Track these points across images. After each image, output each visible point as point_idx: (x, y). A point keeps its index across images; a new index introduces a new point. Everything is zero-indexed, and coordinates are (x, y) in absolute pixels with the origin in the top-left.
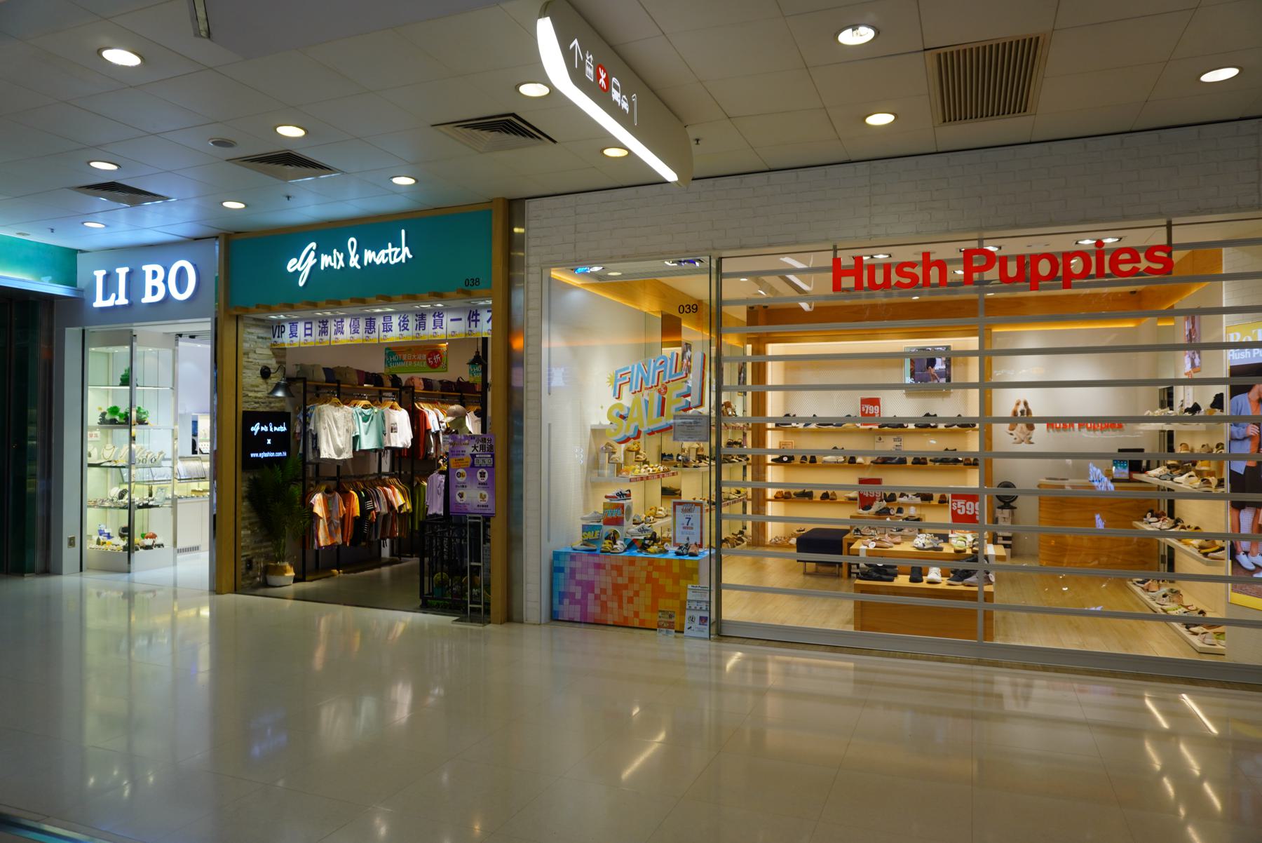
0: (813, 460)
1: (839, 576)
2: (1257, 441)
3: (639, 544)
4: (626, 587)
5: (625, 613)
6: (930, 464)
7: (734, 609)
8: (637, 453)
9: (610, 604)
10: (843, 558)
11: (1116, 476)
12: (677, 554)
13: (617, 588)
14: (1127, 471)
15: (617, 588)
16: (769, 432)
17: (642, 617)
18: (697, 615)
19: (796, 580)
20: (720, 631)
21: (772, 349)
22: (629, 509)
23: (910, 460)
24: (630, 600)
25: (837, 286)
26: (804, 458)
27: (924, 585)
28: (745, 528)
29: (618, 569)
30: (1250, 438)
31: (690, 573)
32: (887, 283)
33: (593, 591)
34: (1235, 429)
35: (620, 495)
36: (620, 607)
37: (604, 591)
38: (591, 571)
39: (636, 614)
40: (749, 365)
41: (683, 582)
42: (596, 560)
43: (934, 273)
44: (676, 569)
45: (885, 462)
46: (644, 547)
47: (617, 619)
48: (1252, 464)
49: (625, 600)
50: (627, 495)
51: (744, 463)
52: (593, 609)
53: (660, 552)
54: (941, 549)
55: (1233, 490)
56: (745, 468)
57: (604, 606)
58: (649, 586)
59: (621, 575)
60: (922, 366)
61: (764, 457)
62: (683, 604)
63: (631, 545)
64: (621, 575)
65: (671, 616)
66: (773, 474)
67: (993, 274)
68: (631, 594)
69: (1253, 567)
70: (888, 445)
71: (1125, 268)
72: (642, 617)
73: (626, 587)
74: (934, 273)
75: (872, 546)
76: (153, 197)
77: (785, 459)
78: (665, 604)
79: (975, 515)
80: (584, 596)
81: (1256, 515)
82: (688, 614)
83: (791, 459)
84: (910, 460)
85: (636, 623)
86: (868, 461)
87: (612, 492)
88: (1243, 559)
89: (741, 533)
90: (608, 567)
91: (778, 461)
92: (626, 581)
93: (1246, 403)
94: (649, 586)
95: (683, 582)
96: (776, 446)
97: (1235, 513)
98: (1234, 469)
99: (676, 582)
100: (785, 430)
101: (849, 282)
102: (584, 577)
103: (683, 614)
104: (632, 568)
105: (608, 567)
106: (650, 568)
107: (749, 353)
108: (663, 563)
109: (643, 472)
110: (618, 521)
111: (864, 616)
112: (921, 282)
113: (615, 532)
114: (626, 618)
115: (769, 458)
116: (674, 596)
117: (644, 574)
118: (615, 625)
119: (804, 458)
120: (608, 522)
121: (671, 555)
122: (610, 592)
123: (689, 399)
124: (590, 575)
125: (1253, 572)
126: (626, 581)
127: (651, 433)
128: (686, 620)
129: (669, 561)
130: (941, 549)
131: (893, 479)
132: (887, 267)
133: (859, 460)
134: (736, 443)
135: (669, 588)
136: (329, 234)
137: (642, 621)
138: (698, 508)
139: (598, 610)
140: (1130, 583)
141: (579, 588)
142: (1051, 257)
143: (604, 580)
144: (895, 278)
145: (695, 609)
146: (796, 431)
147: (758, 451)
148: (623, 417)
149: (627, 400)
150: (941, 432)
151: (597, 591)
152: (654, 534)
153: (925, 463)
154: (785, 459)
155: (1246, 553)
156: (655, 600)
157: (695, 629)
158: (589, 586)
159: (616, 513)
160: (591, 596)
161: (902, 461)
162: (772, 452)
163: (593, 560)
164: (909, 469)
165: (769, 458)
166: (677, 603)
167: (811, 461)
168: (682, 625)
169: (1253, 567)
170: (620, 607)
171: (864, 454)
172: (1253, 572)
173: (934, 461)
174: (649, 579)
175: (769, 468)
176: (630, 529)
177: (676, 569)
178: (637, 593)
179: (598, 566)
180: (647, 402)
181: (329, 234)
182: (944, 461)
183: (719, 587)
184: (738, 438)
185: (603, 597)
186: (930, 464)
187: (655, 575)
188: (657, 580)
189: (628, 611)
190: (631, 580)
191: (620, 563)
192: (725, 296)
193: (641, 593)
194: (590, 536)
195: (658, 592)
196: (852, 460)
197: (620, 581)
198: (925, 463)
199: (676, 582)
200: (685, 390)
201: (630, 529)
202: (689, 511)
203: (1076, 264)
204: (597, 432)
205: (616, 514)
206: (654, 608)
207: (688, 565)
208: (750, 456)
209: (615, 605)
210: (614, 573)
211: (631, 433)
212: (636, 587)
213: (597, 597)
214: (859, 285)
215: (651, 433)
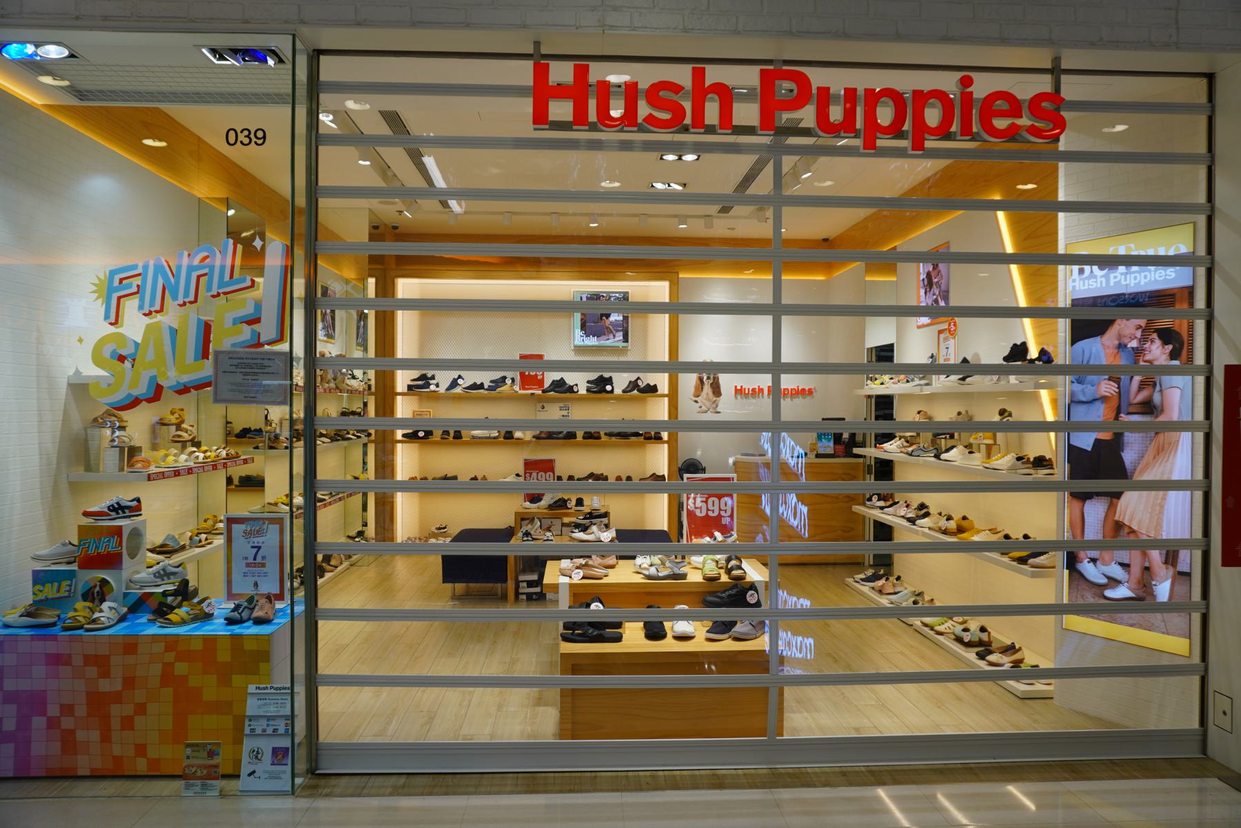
0: (458, 435)
1: (504, 598)
2: (1115, 403)
3: (153, 603)
4: (117, 698)
5: (117, 750)
6: (604, 438)
7: (345, 714)
8: (178, 427)
9: (80, 735)
11: (821, 451)
12: (230, 621)
13: (98, 703)
14: (832, 444)
15: (98, 703)
16: (399, 398)
17: (152, 753)
18: (266, 746)
19: (443, 604)
20: (315, 766)
21: (406, 287)
22: (137, 534)
23: (580, 435)
24: (128, 723)
25: (540, 117)
26: (446, 433)
27: (668, 645)
28: (365, 525)
29: (101, 663)
30: (1104, 399)
31: (252, 659)
32: (630, 118)
33: (43, 713)
34: (1077, 387)
35: (118, 509)
36: (106, 738)
37: (68, 709)
38: (40, 670)
39: (141, 750)
40: (371, 315)
41: (237, 680)
42: (51, 647)
43: (712, 112)
44: (224, 656)
45: (549, 436)
46: (162, 611)
47: (98, 764)
48: (1105, 436)
49: (115, 723)
50: (135, 508)
51: (364, 439)
52: (43, 747)
53: (195, 619)
54: (684, 576)
55: (1073, 475)
56: (365, 445)
57: (69, 743)
58: (168, 693)
59: (105, 674)
60: (595, 317)
61: (393, 433)
62: (240, 720)
63: (138, 605)
64: (105, 674)
65: (211, 754)
66: (406, 461)
67: (807, 116)
68: (128, 710)
69: (1104, 581)
70: (553, 414)
71: (1001, 123)
72: (152, 753)
73: (117, 698)
74: (712, 112)
75: (577, 577)
76: (1080, 713)
77: (421, 434)
78: (203, 727)
79: (720, 517)
80: (24, 723)
81: (1112, 508)
82: (248, 745)
83: (429, 433)
84: (580, 435)
85: (142, 766)
86: (528, 436)
87: (100, 505)
88: (1088, 569)
89: (361, 534)
90: (78, 661)
91: (412, 437)
92: (118, 686)
93: (1099, 349)
94: (168, 693)
95: (237, 680)
96: (408, 415)
97: (1077, 504)
98: (1074, 442)
99: (224, 680)
100: (419, 394)
101: (561, 110)
102: (24, 685)
103: (238, 741)
104: (130, 659)
105: (78, 661)
106: (170, 657)
107: (371, 293)
108: (198, 646)
109: (183, 460)
110: (112, 561)
111: (580, 714)
112: (688, 120)
113: (104, 582)
114: (118, 760)
115: (399, 434)
116: (221, 707)
117: (157, 669)
118: (96, 776)
119: (446, 433)
120: (90, 562)
121: (218, 627)
122: (81, 711)
123: (256, 327)
124: (38, 678)
125: (1104, 587)
126: (118, 686)
127: (183, 390)
128: (245, 758)
129: (210, 641)
130: (684, 576)
131: (574, 461)
132: (631, 91)
133: (518, 434)
134: (353, 413)
135: (210, 688)
136: (479, 485)
137: (154, 763)
138: (275, 528)
139: (56, 747)
140: (850, 580)
141: (12, 709)
142: (895, 96)
143: (67, 688)
144: (643, 110)
145: (264, 734)
146: (435, 396)
147: (384, 422)
148: (122, 359)
149: (134, 326)
150: (618, 398)
151: (53, 710)
152: (185, 583)
153: (599, 438)
154: (421, 434)
155: (1094, 560)
156: (180, 720)
157: (262, 773)
158: (34, 703)
159: (107, 546)
160: (38, 722)
161: (571, 436)
162: (403, 423)
163: (41, 647)
164: (579, 445)
165: (399, 434)
166: (227, 721)
167: (455, 436)
168: (238, 763)
169: (1104, 581)
170: (106, 738)
171: (523, 425)
172: (1104, 587)
173: (610, 435)
174: (167, 677)
175: (399, 446)
176: (139, 572)
177: (224, 656)
178: (141, 709)
179: (56, 660)
180: (174, 332)
181: (479, 485)
182: (623, 435)
183: (313, 681)
184: (357, 406)
185: (67, 723)
186: (604, 438)
187: (181, 668)
188: (185, 678)
189: (121, 746)
190: (129, 682)
191: (103, 651)
192: (326, 179)
193: (151, 708)
194: (49, 591)
195: (187, 701)
196: (509, 436)
197: (105, 686)
198: (599, 438)
199: (224, 680)
200: (249, 310)
201: (139, 572)
202: (259, 533)
203: (933, 116)
204: (79, 389)
205: (102, 548)
206: (179, 734)
207: (249, 646)
208: (372, 432)
209: (95, 735)
210: (92, 671)
211: (141, 390)
212: (139, 696)
213: (52, 723)
214: (580, 118)
215: (183, 390)
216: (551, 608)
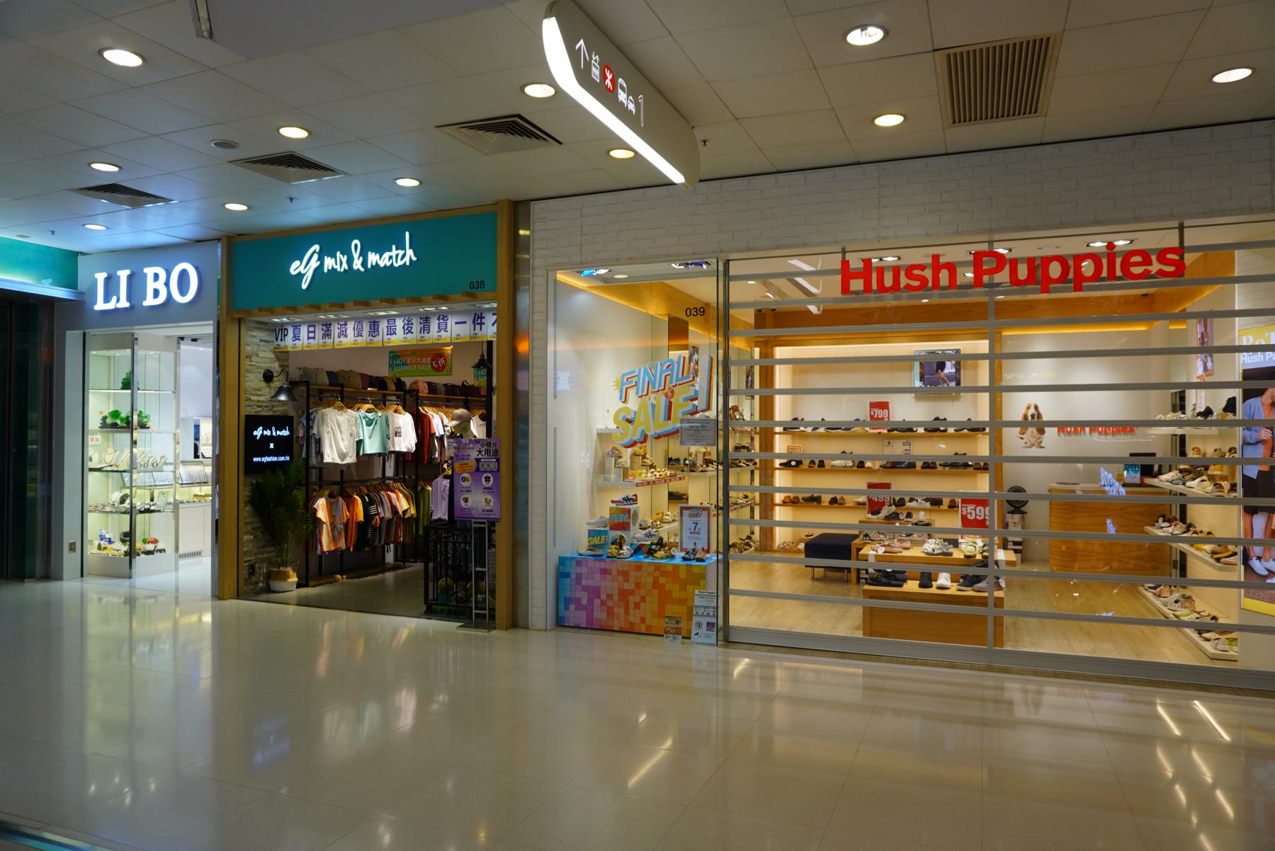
0: (822, 464)
1: (847, 581)
2: (1270, 445)
3: (646, 549)
4: (632, 592)
5: (632, 619)
6: (940, 468)
7: (742, 615)
8: (644, 457)
9: (616, 610)
11: (1128, 481)
12: (684, 559)
13: (624, 594)
14: (1138, 475)
15: (624, 594)
16: (777, 437)
17: (648, 622)
18: (704, 621)
19: (804, 585)
20: (727, 637)
21: (780, 352)
22: (636, 514)
23: (919, 465)
24: (637, 606)
25: (845, 289)
26: (812, 462)
27: (933, 590)
28: (753, 533)
29: (625, 574)
30: (1263, 442)
31: (697, 579)
32: (896, 286)
33: (599, 597)
34: (1247, 433)
35: (627, 499)
36: (627, 613)
37: (610, 597)
38: (598, 576)
39: (643, 620)
40: (757, 369)
41: (690, 588)
42: (602, 565)
43: (944, 276)
44: (683, 575)
45: (894, 466)
46: (651, 552)
47: (623, 625)
48: (1265, 468)
49: (631, 606)
50: (633, 500)
51: (752, 467)
52: (600, 615)
53: (667, 557)
54: (951, 554)
55: (1246, 494)
56: (752, 472)
57: (610, 612)
58: (655, 592)
59: (627, 580)
60: (932, 369)
61: (772, 462)
62: (690, 610)
63: (638, 550)
64: (627, 580)
65: (678, 622)
66: (781, 479)
67: (1003, 277)
68: (637, 599)
69: (1266, 573)
70: (897, 449)
71: (1137, 270)
72: (648, 622)
73: (632, 592)
74: (944, 276)
75: (881, 551)
77: (793, 463)
78: (671, 609)
79: (985, 520)
80: (590, 602)
81: (1269, 520)
82: (695, 619)
83: (799, 463)
84: (919, 465)
85: (643, 629)
86: (877, 465)
87: (619, 497)
88: (1256, 564)
89: (749, 538)
90: (614, 572)
91: (786, 466)
92: (632, 586)
93: (1259, 407)
94: (655, 592)
95: (690, 588)
96: (784, 450)
97: (1248, 517)
98: (1246, 473)
99: (683, 588)
100: (793, 434)
101: (857, 285)
102: (590, 583)
103: (690, 619)
104: (638, 574)
105: (614, 572)
106: (657, 574)
107: (757, 356)
108: (670, 569)
109: (650, 477)
110: (624, 526)
111: (873, 621)
112: (930, 284)
113: (622, 537)
114: (632, 624)
115: (777, 463)
116: (681, 601)
117: (650, 580)
118: (621, 631)
119: (812, 462)
120: (615, 527)
121: (678, 561)
122: (616, 598)
123: (696, 403)
124: (596, 581)
125: (1265, 577)
126: (632, 586)
127: (658, 437)
128: (694, 626)
129: (676, 567)
130: (951, 554)
131: (903, 484)
132: (896, 270)
133: (868, 464)
134: (743, 447)
135: (676, 593)
136: (333, 236)
137: (649, 627)
138: (705, 513)
139: (604, 615)
140: (1141, 589)
141: (585, 594)
142: (1061, 260)
143: (610, 586)
144: (904, 281)
145: (702, 615)
146: (804, 435)
147: (766, 455)
148: (630, 421)
149: (633, 404)
150: (951, 436)
151: (603, 597)
152: (661, 539)
153: (935, 468)
154: (793, 463)
155: (1259, 558)
156: (661, 606)
157: (702, 635)
158: (595, 592)
159: (623, 518)
160: (597, 602)
161: (912, 466)
162: (780, 456)
163: (599, 565)
164: (918, 473)
165: (777, 463)
166: (684, 609)
167: (819, 465)
168: (689, 631)
169: (1266, 573)
170: (627, 613)
171: (873, 458)
172: (1265, 577)
173: (944, 465)
174: (656, 584)
175: (777, 472)
176: (636, 534)
177: (683, 575)
178: (643, 599)
179: (604, 572)
180: (653, 406)
181: (333, 236)
182: (954, 465)
183: (727, 592)
184: (746, 442)
185: (610, 603)
186: (940, 468)
187: (662, 580)
188: (664, 585)
189: (634, 617)
190: (638, 585)
191: (626, 569)
193: (648, 599)
194: (596, 541)
195: (665, 597)
196: (861, 465)
197: (626, 586)
198: (935, 468)
199: (683, 588)
200: (692, 394)
201: (636, 534)
202: (697, 515)
203: (1087, 267)
204: (603, 436)
205: (622, 519)
206: (661, 614)
207: (696, 571)
208: (757, 461)
209: (622, 611)
210: (621, 578)
211: (637, 437)
212: (642, 592)
213: (603, 603)
214: (868, 288)
215: (658, 437)
216: (852, 564)
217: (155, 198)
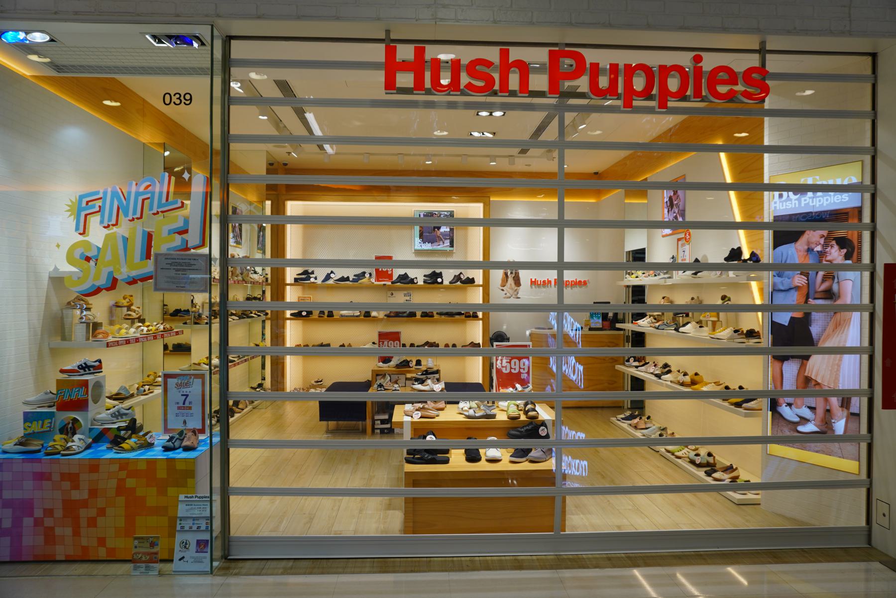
0: (331, 314)
1: (364, 432)
2: (805, 291)
3: (110, 436)
4: (85, 504)
5: (84, 542)
6: (436, 317)
7: (249, 516)
8: (129, 308)
9: (58, 531)
10: (398, 439)
11: (593, 326)
12: (166, 449)
13: (71, 508)
14: (600, 321)
15: (71, 508)
16: (288, 287)
17: (110, 544)
18: (192, 538)
19: (320, 436)
20: (228, 553)
21: (293, 207)
22: (99, 386)
23: (419, 314)
24: (92, 522)
25: (390, 85)
26: (322, 312)
27: (482, 466)
28: (264, 379)
29: (73, 479)
30: (797, 288)
31: (182, 476)
32: (455, 85)
33: (31, 515)
34: (778, 280)
35: (85, 368)
36: (76, 533)
37: (49, 512)
38: (29, 484)
39: (102, 542)
40: (268, 227)
41: (171, 491)
42: (37, 467)
43: (514, 81)
44: (162, 474)
45: (396, 315)
46: (117, 441)
47: (71, 551)
48: (798, 315)
49: (83, 523)
50: (97, 367)
51: (263, 317)
52: (31, 540)
53: (141, 447)
54: (494, 416)
55: (775, 343)
56: (264, 322)
57: (50, 537)
58: (121, 500)
59: (76, 487)
60: (430, 229)
61: (284, 313)
62: (173, 520)
63: (99, 437)
64: (76, 487)
65: (153, 545)
66: (293, 333)
67: (583, 83)
68: (93, 512)
69: (797, 419)
70: (399, 299)
71: (722, 89)
72: (110, 544)
73: (85, 504)
74: (514, 81)
75: (417, 417)
77: (304, 314)
78: (146, 525)
79: (519, 373)
80: (17, 522)
81: (803, 367)
82: (179, 538)
83: (309, 313)
84: (419, 314)
85: (102, 553)
86: (381, 315)
87: (72, 365)
88: (785, 411)
89: (260, 385)
90: (56, 477)
91: (297, 316)
92: (85, 496)
93: (793, 252)
94: (121, 500)
95: (171, 491)
96: (295, 300)
97: (777, 364)
98: (776, 319)
99: (162, 491)
100: (303, 285)
101: (405, 79)
102: (17, 495)
103: (172, 535)
104: (94, 476)
105: (56, 477)
106: (123, 474)
107: (268, 211)
108: (143, 466)
109: (132, 332)
110: (81, 405)
111: (418, 516)
112: (497, 87)
113: (75, 420)
114: (85, 549)
115: (288, 314)
116: (159, 511)
117: (113, 483)
118: (69, 561)
119: (322, 312)
120: (65, 406)
121: (157, 453)
122: (58, 513)
123: (185, 236)
124: (28, 490)
125: (797, 424)
126: (85, 496)
127: (132, 282)
128: (177, 548)
129: (152, 463)
130: (494, 416)
131: (414, 333)
132: (455, 66)
133: (374, 314)
134: (255, 298)
135: (151, 497)
136: (346, 350)
137: (111, 551)
138: (198, 381)
139: (41, 540)
140: (614, 419)
141: (8, 512)
142: (646, 70)
143: (49, 497)
144: (465, 79)
145: (190, 530)
146: (314, 286)
147: (277, 305)
148: (88, 259)
149: (97, 235)
150: (446, 288)
151: (38, 513)
152: (134, 421)
153: (433, 316)
154: (304, 314)
155: (790, 405)
156: (130, 520)
157: (189, 558)
158: (25, 507)
159: (77, 394)
160: (28, 522)
161: (412, 315)
162: (291, 306)
163: (29, 468)
164: (418, 321)
165: (288, 314)
166: (164, 521)
167: (328, 315)
168: (171, 551)
169: (797, 419)
170: (76, 533)
171: (378, 307)
172: (797, 424)
173: (440, 314)
174: (121, 489)
175: (288, 322)
176: (101, 413)
177: (162, 474)
178: (102, 512)
179: (41, 477)
180: (125, 240)
181: (346, 350)
182: (450, 314)
183: (226, 492)
184: (258, 293)
185: (49, 522)
186: (436, 317)
187: (131, 483)
188: (133, 490)
189: (87, 539)
190: (93, 493)
191: (75, 470)
193: (109, 511)
194: (36, 427)
195: (135, 506)
196: (367, 315)
197: (75, 495)
198: (433, 316)
199: (162, 491)
200: (180, 224)
201: (101, 413)
202: (187, 385)
204: (57, 281)
205: (73, 396)
206: (129, 530)
207: (180, 466)
208: (269, 312)
209: (69, 531)
210: (67, 485)
211: (102, 281)
212: (101, 502)
213: (38, 522)
214: (419, 85)
215: (132, 282)
217: (780, 515)
